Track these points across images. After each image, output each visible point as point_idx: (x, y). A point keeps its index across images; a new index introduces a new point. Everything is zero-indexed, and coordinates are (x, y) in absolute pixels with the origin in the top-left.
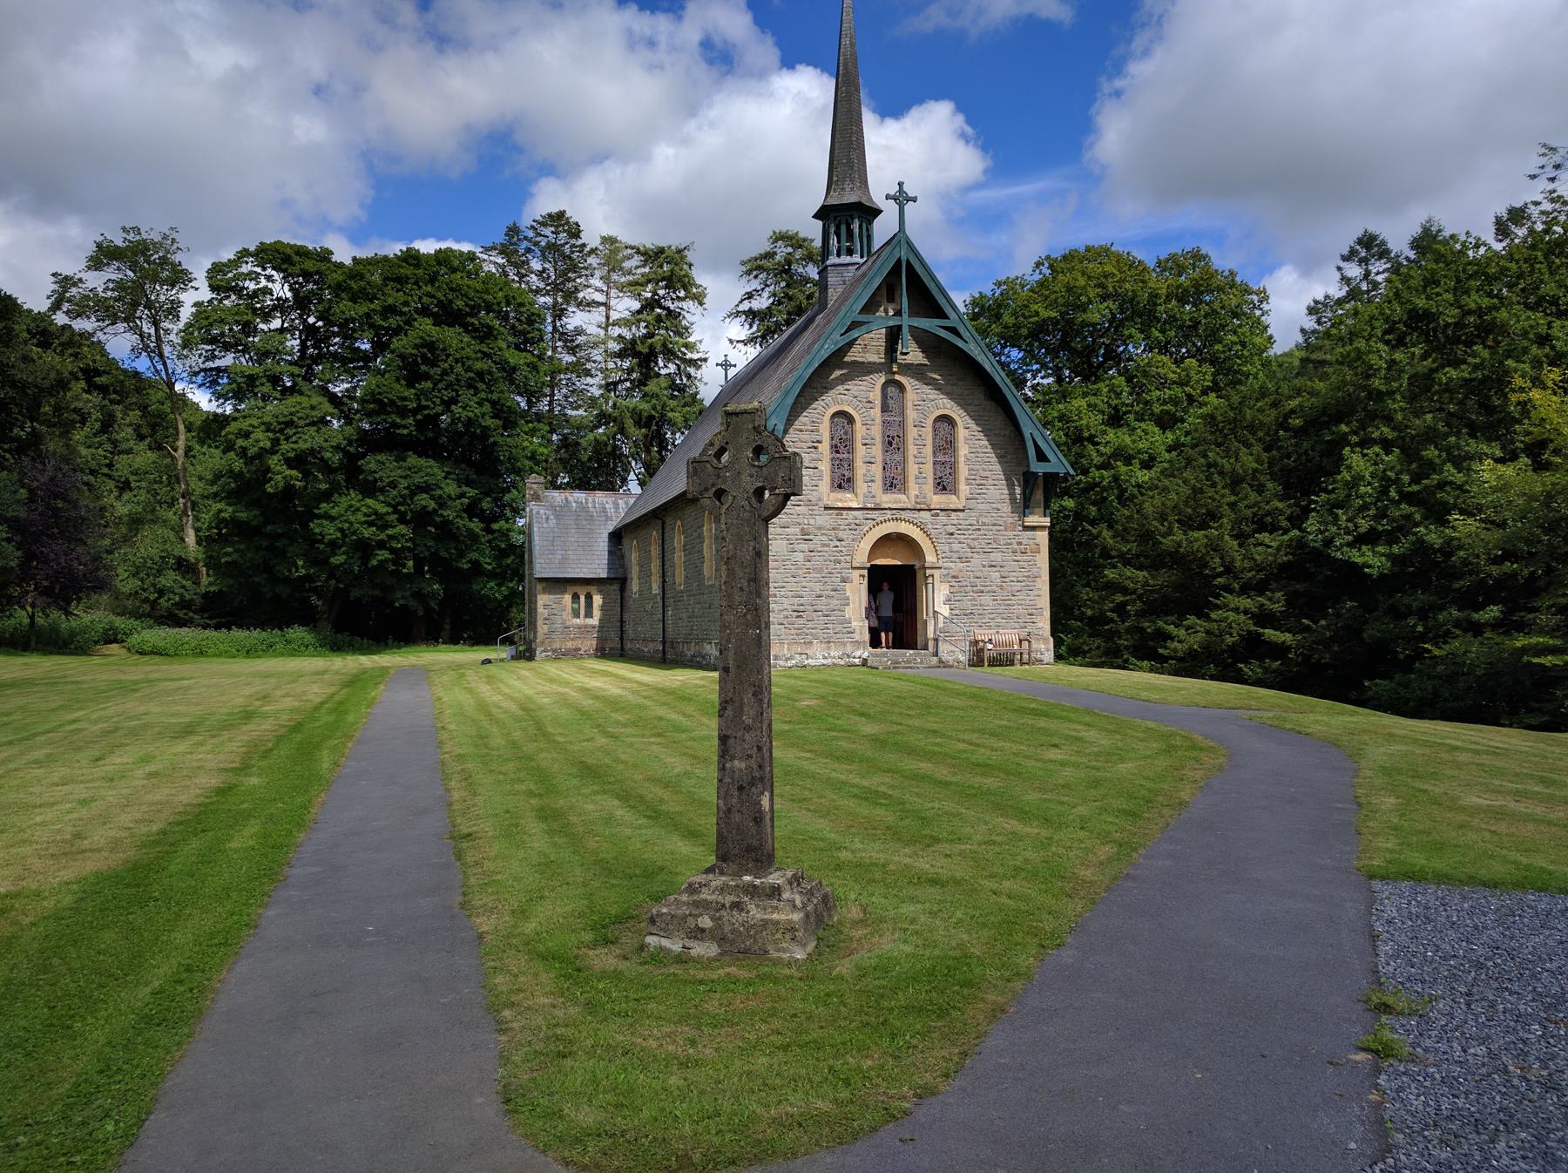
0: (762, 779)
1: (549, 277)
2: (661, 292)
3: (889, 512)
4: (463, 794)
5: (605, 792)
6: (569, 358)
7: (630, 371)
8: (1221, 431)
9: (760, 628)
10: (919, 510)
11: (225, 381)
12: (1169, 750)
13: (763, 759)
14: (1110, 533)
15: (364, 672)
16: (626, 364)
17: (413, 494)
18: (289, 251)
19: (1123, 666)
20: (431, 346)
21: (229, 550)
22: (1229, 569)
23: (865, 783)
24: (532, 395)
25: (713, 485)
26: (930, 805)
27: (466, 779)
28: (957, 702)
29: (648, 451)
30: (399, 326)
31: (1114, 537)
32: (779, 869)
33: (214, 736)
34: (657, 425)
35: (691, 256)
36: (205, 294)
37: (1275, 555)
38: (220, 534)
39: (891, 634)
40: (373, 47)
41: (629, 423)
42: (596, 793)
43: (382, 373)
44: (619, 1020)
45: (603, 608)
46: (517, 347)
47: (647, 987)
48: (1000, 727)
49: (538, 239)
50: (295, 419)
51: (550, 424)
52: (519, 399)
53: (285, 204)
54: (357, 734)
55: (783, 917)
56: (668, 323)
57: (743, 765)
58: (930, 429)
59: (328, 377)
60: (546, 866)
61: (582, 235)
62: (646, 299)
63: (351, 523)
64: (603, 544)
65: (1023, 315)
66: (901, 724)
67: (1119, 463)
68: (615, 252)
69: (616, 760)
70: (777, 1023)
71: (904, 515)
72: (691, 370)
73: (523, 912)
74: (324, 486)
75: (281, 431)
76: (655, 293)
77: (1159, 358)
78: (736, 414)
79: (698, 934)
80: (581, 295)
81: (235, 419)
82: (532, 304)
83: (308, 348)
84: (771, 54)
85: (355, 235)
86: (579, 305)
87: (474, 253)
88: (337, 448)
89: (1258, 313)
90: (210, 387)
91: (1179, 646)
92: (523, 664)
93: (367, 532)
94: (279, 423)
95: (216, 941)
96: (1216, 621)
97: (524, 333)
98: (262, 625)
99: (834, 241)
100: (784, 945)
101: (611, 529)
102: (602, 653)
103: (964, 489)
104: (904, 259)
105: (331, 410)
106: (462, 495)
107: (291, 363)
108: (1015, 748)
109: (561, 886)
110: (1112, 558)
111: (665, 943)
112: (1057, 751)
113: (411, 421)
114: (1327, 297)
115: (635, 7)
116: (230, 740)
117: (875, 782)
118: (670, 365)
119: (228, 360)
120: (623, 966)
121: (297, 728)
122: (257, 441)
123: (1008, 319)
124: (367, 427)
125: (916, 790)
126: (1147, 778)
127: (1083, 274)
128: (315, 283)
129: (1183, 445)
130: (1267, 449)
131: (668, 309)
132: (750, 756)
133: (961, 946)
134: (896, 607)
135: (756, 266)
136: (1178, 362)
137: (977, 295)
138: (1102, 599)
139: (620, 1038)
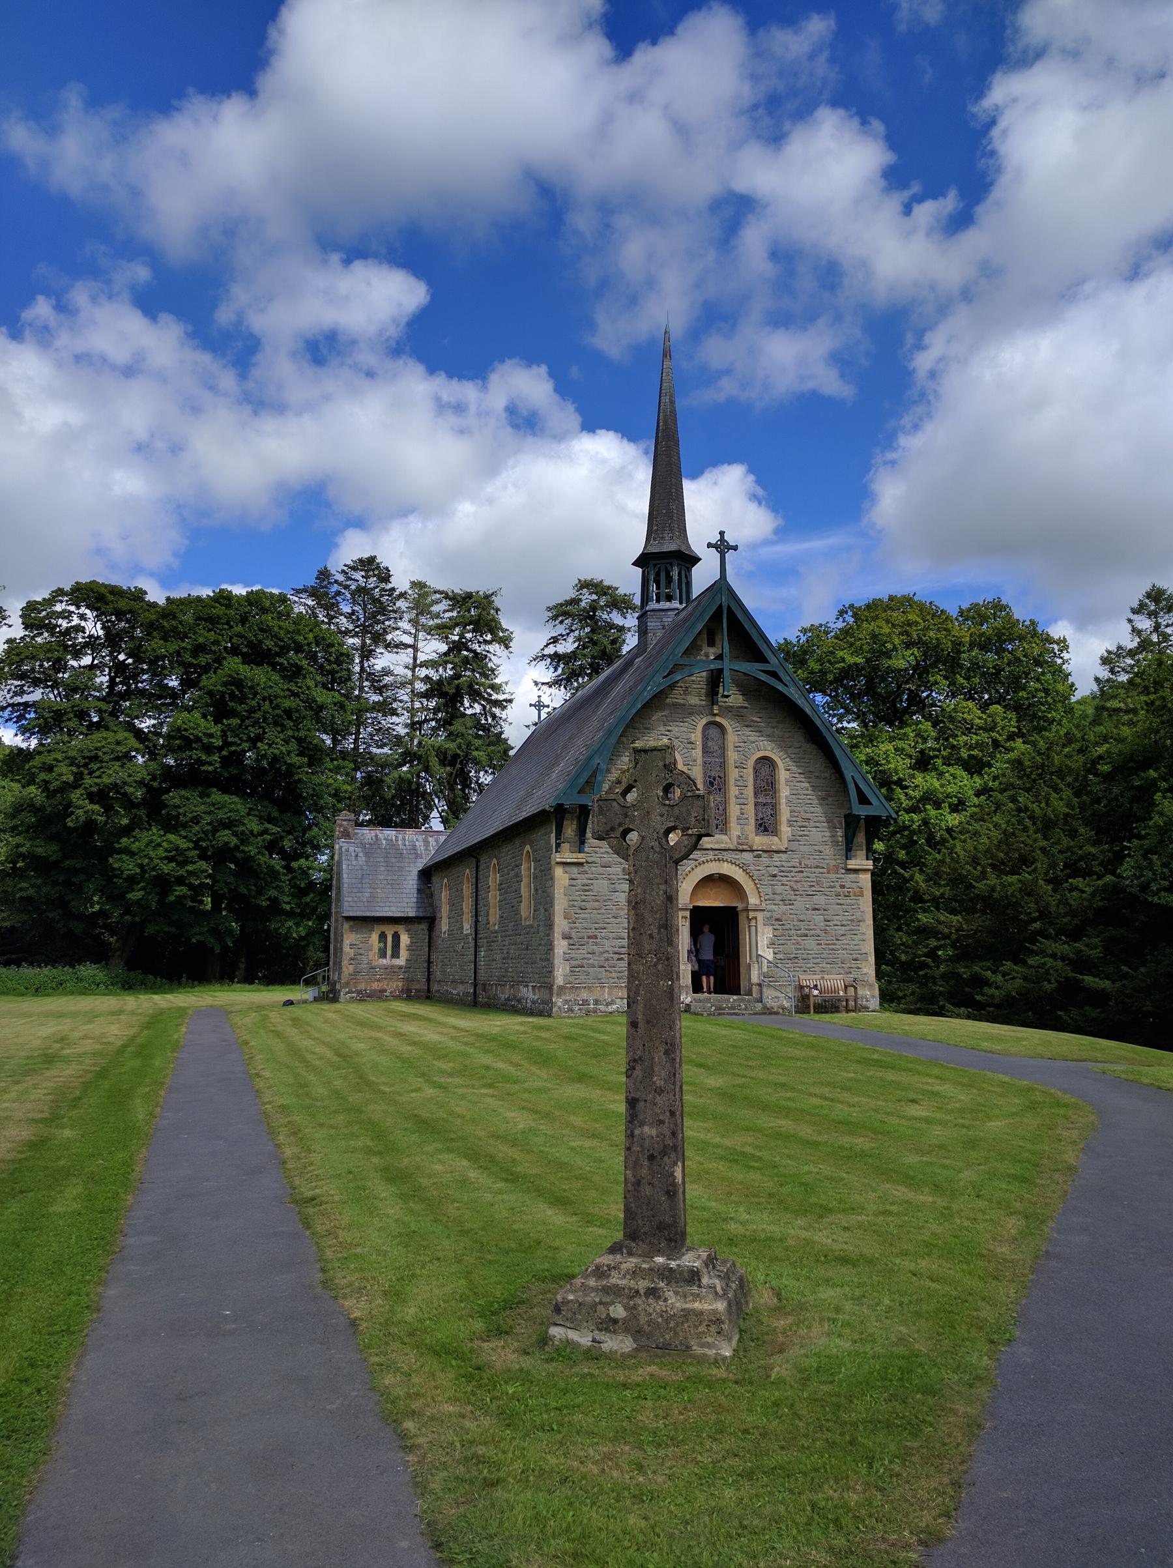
0: (675, 1148)
1: (358, 619)
2: (469, 635)
3: (711, 852)
4: (296, 1150)
5: (450, 1150)
6: (376, 698)
7: (436, 710)
8: (1028, 776)
9: (671, 979)
10: (742, 851)
11: (33, 715)
12: (1033, 1107)
13: (676, 1125)
14: (922, 877)
15: (161, 1012)
16: (432, 704)
17: (215, 830)
18: (103, 590)
19: (940, 1013)
20: (238, 683)
21: (24, 885)
22: (1043, 915)
23: (727, 1142)
24: (337, 734)
25: (620, 825)
26: (806, 1168)
27: (295, 1133)
28: (797, 1052)
29: (452, 789)
30: (208, 664)
31: (927, 881)
32: (690, 1249)
33: (17, 1082)
34: (461, 763)
35: (497, 601)
36: (17, 631)
37: (1089, 901)
38: (14, 868)
39: (712, 978)
40: (195, 409)
41: (434, 762)
42: (440, 1151)
43: (189, 710)
44: (545, 1436)
45: (410, 948)
46: (324, 686)
47: (565, 1391)
48: (850, 1079)
49: (348, 583)
50: (100, 754)
51: (355, 762)
52: (324, 737)
53: (99, 552)
54: (168, 1081)
55: (706, 1307)
56: (474, 665)
57: (654, 1132)
58: (751, 771)
59: (135, 713)
60: (408, 1238)
61: (392, 579)
62: (454, 642)
63: (151, 859)
64: (411, 882)
65: (829, 661)
66: (744, 1076)
67: (928, 807)
68: (423, 596)
69: (451, 1113)
70: (729, 1442)
71: (726, 855)
72: (497, 711)
73: (398, 1294)
74: (125, 821)
75: (86, 765)
76: (462, 636)
77: (964, 704)
78: (645, 751)
79: (610, 1325)
80: (389, 637)
81: (40, 753)
82: (342, 644)
83: (117, 684)
84: (575, 420)
85: (165, 581)
86: (388, 646)
87: (285, 596)
88: (141, 783)
89: (1059, 661)
90: (16, 722)
91: (996, 992)
92: (326, 1006)
93: (167, 868)
94: (84, 758)
95: (57, 1328)
96: (1032, 967)
97: (332, 673)
98: (52, 961)
99: (653, 587)
100: (709, 1340)
101: (420, 866)
102: (408, 995)
103: (785, 830)
104: (725, 604)
105: (137, 745)
106: (265, 832)
107: (98, 699)
108: (873, 1103)
109: (430, 1261)
110: (923, 901)
111: (573, 1335)
112: (917, 1107)
113: (216, 758)
114: (1120, 648)
115: (443, 375)
116: (35, 1087)
117: (736, 1141)
118: (476, 705)
119: (36, 695)
120: (527, 1362)
121: (103, 1074)
122: (61, 775)
123: (813, 665)
124: (172, 762)
125: (786, 1151)
126: (1023, 1138)
127: (888, 622)
128: (128, 621)
129: (991, 789)
130: (1077, 794)
131: (474, 652)
132: (661, 1122)
133: (902, 1340)
134: (718, 949)
135: (561, 612)
136: (984, 707)
137: (782, 642)
138: (916, 943)
139: (553, 1461)
